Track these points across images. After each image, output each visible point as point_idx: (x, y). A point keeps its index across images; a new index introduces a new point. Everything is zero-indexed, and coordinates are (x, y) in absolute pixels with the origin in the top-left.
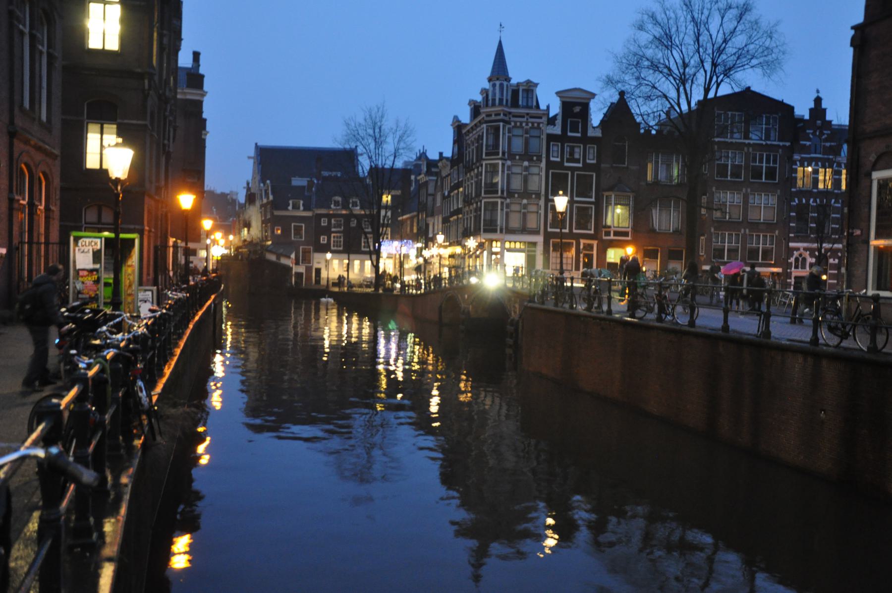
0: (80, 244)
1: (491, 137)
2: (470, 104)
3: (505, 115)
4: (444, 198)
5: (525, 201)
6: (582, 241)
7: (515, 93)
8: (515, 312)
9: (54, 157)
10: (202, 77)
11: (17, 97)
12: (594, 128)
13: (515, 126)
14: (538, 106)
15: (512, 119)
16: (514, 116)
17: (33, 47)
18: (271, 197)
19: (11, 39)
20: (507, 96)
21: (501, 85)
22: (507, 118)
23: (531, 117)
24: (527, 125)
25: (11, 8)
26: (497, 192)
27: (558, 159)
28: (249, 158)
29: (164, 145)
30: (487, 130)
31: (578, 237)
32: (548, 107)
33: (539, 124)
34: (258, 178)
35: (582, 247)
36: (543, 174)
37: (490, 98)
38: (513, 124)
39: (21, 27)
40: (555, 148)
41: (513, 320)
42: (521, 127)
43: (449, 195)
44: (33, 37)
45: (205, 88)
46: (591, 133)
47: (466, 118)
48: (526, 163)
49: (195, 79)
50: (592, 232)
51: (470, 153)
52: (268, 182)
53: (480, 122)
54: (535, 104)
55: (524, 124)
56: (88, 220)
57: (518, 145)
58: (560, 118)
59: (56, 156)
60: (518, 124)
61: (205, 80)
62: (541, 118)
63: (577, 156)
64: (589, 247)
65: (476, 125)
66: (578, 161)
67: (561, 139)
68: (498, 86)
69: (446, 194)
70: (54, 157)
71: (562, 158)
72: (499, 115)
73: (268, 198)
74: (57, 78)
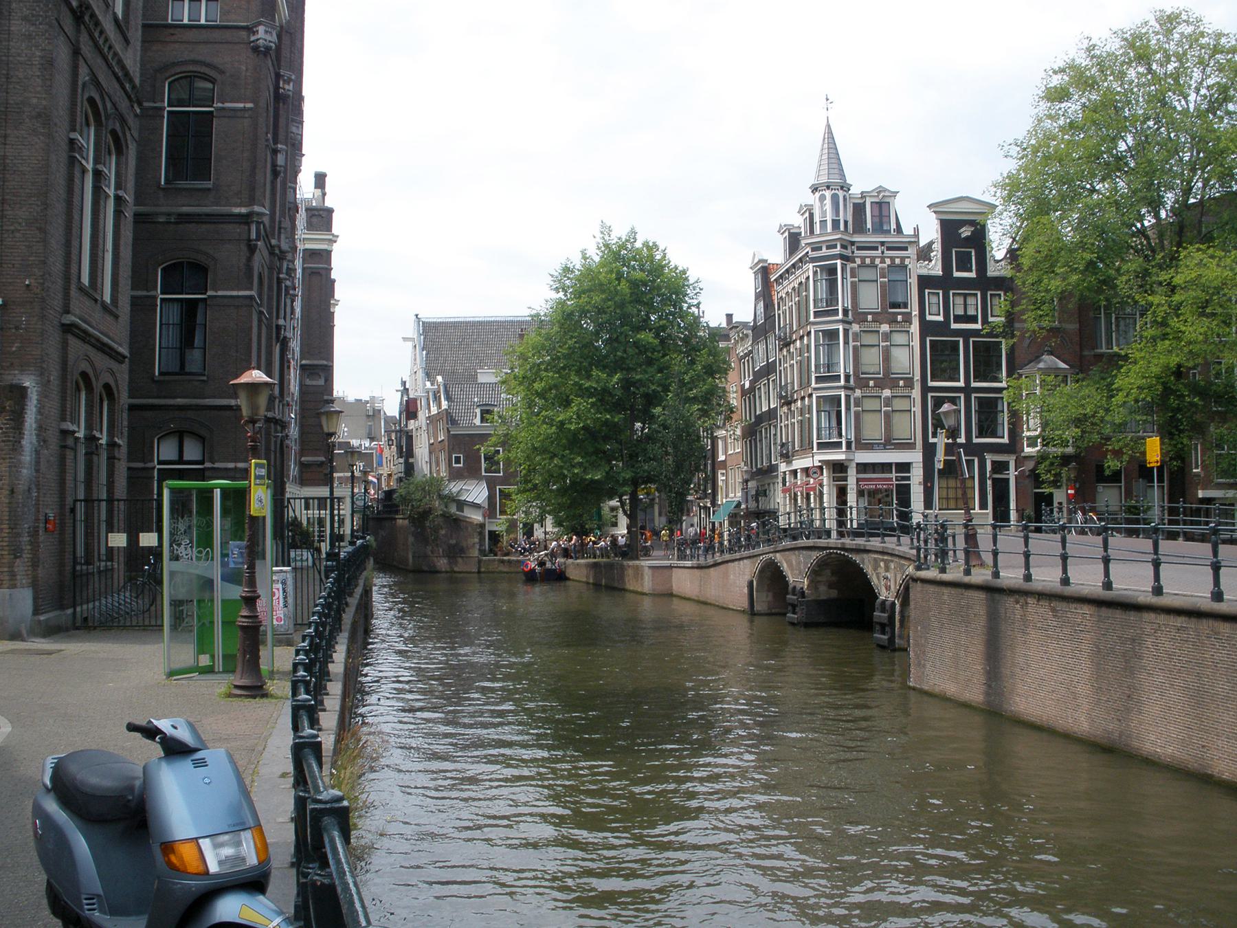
0: (1160, 387)
1: (823, 286)
2: (781, 230)
3: (843, 247)
4: (744, 393)
5: (887, 393)
6: (989, 458)
7: (859, 209)
8: (888, 588)
9: (119, 358)
10: (330, 211)
11: (74, 270)
12: (998, 261)
13: (863, 265)
14: (899, 229)
15: (857, 253)
16: (859, 248)
17: (97, 189)
18: (445, 404)
19: (70, 180)
20: (846, 215)
21: (835, 199)
22: (848, 253)
23: (889, 249)
24: (883, 262)
25: (73, 135)
26: (837, 378)
27: (941, 318)
28: (405, 339)
29: (278, 328)
30: (815, 273)
31: (979, 451)
32: (916, 230)
33: (903, 259)
34: (421, 374)
35: (989, 468)
36: (916, 343)
37: (817, 219)
38: (858, 261)
39: (84, 162)
40: (934, 300)
41: (884, 602)
42: (873, 266)
43: (752, 389)
44: (98, 174)
45: (335, 230)
46: (992, 271)
47: (776, 255)
48: (885, 328)
49: (321, 218)
50: (1006, 440)
51: (786, 314)
52: (440, 378)
53: (801, 260)
54: (893, 226)
55: (877, 261)
56: (161, 458)
57: (870, 299)
58: (937, 247)
59: (124, 357)
60: (868, 261)
61: (336, 217)
62: (906, 249)
63: (971, 312)
64: (1000, 467)
65: (794, 266)
66: (973, 319)
67: (944, 283)
68: (828, 202)
69: (747, 386)
70: (119, 358)
71: (947, 315)
72: (835, 247)
73: (439, 406)
74: (128, 234)
